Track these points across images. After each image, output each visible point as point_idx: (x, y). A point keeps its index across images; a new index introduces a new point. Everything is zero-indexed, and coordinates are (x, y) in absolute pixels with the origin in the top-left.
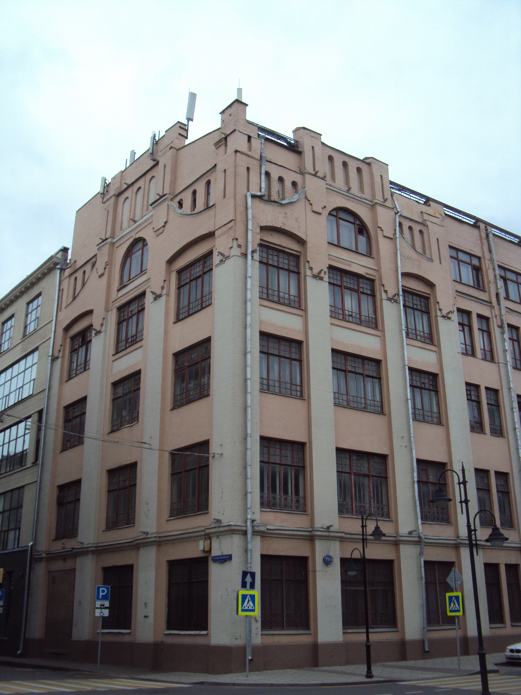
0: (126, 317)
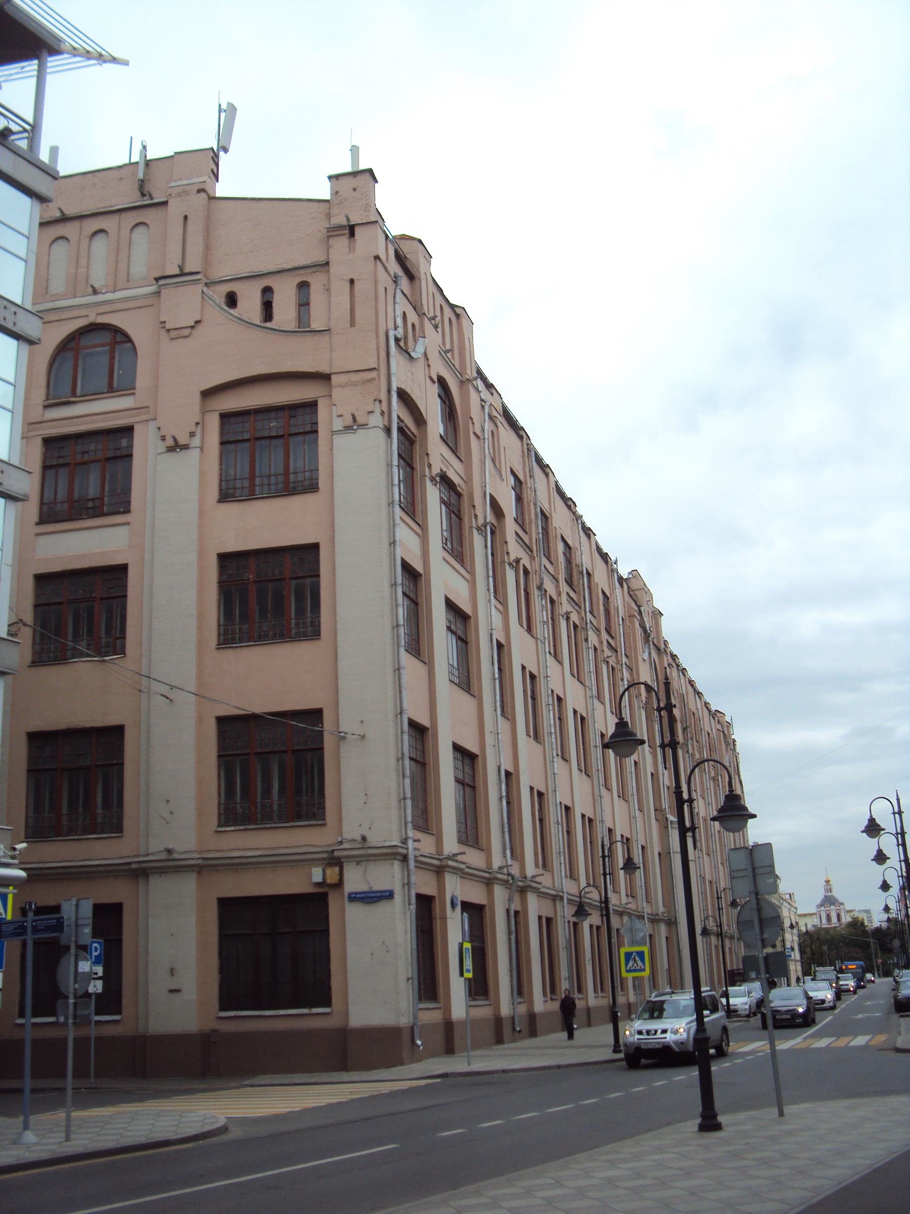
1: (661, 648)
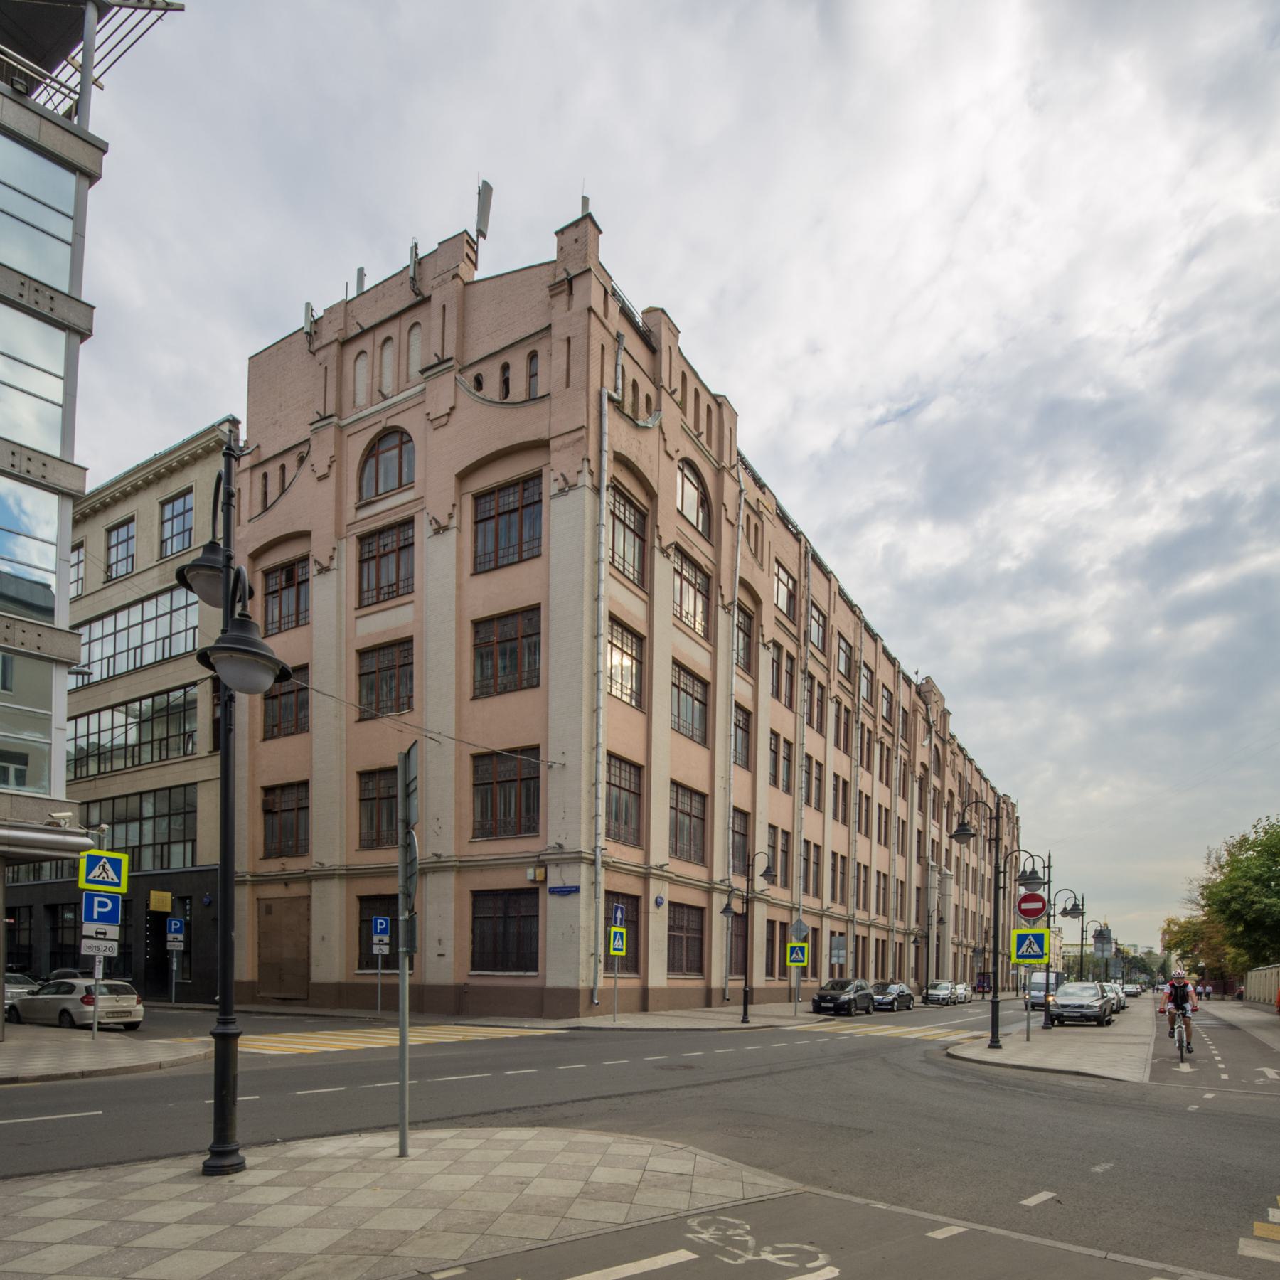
0: (375, 553)
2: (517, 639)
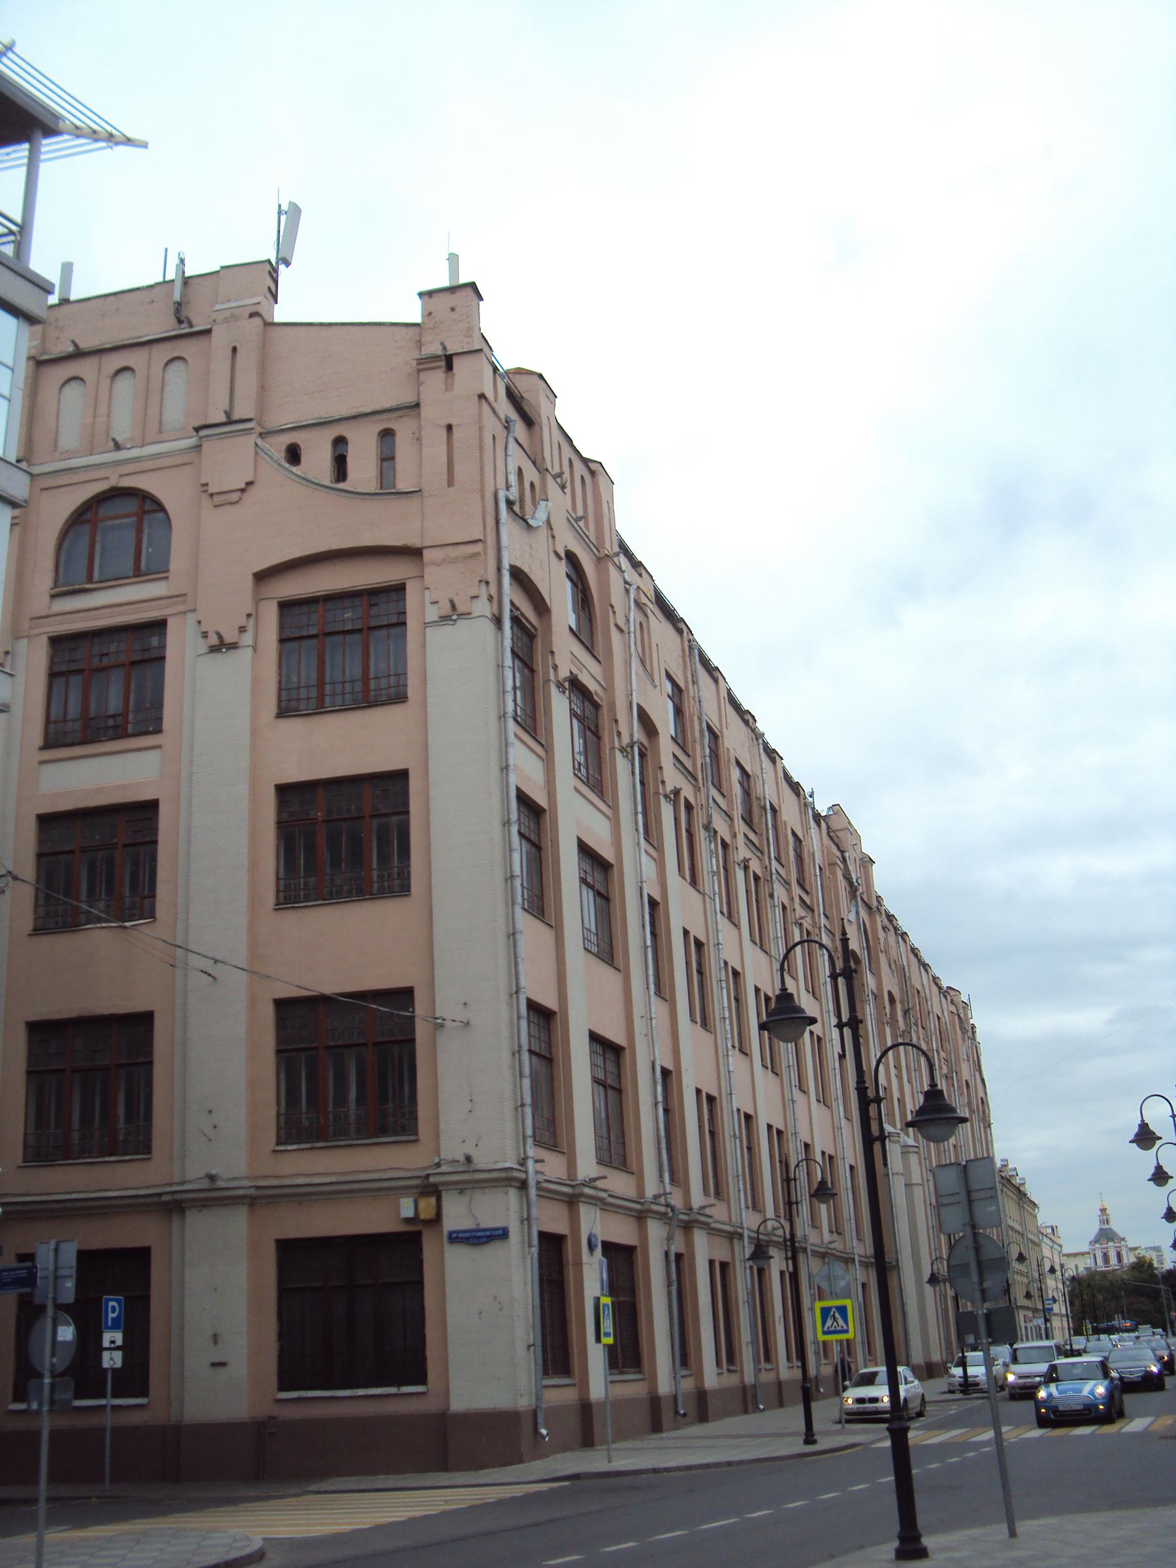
1: (874, 906)
2: (363, 817)
